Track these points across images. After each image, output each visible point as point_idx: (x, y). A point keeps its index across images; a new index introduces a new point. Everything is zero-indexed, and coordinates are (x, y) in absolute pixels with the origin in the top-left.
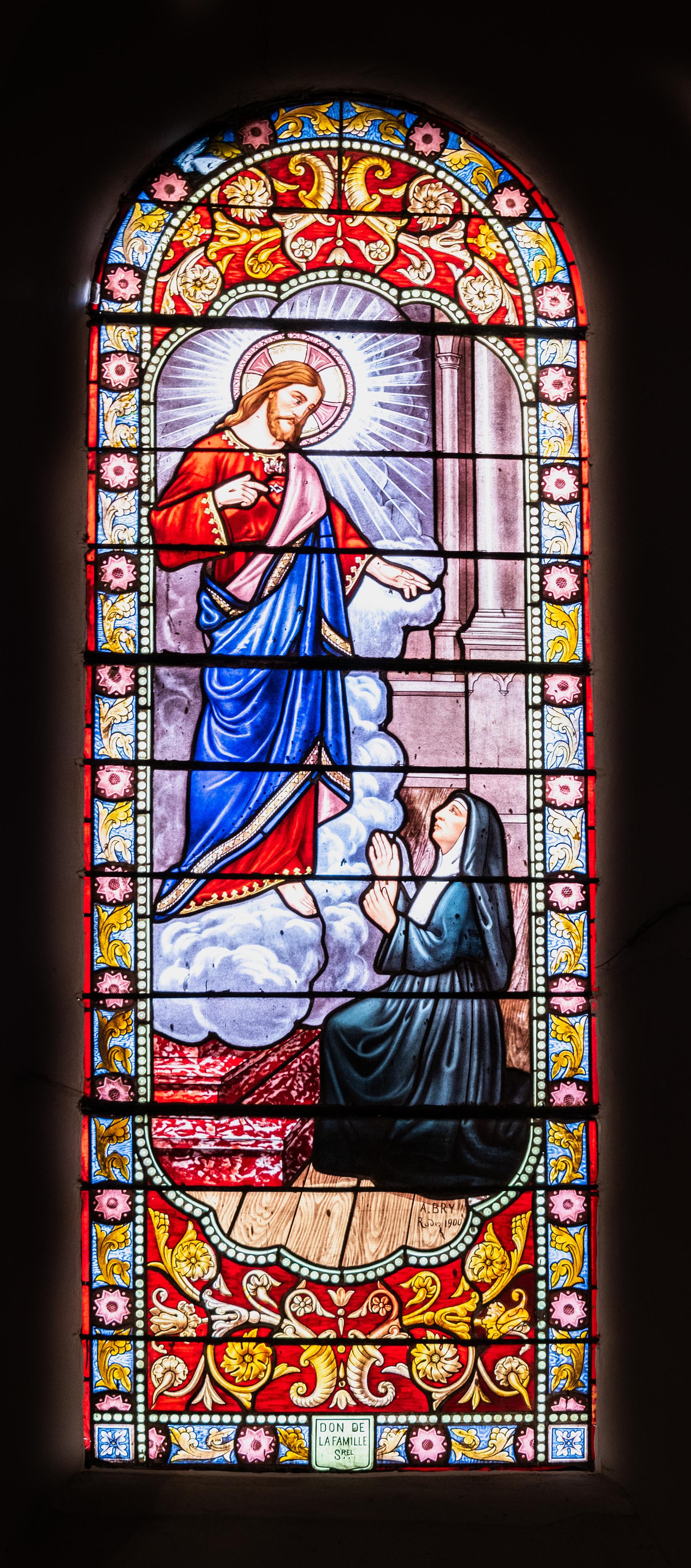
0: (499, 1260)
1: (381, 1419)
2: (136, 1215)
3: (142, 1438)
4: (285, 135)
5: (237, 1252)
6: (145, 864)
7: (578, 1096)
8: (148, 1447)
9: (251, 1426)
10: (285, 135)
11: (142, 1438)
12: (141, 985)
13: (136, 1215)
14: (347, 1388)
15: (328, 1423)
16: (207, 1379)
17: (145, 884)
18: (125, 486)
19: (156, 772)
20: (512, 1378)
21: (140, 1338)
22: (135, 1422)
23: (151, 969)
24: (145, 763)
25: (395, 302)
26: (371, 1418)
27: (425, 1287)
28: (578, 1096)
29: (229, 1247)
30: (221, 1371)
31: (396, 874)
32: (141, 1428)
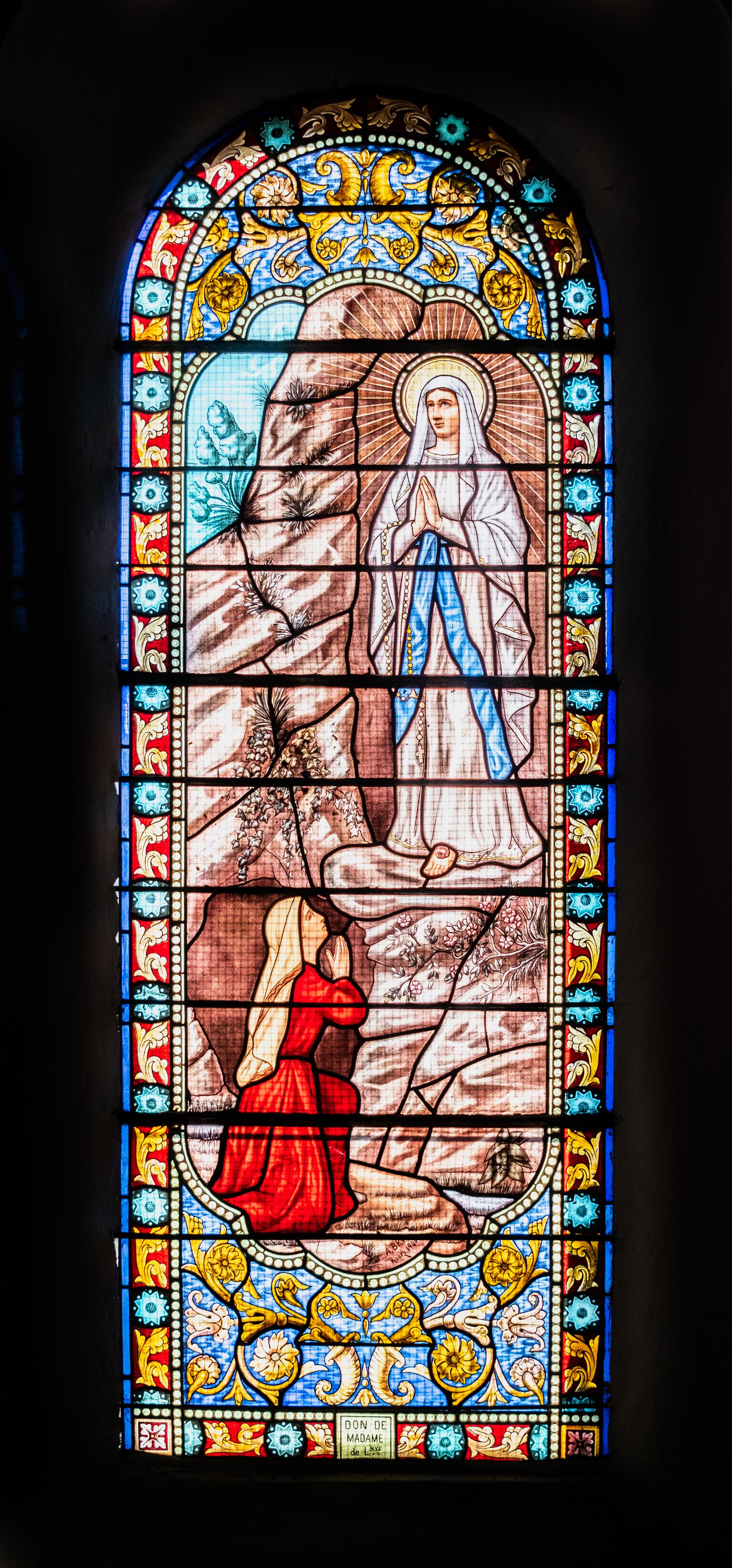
0: (516, 1264)
1: (401, 1417)
2: (173, 1320)
3: (178, 1432)
4: (308, 135)
5: (266, 1256)
6: (180, 768)
7: (591, 1102)
8: (184, 1441)
9: (280, 1422)
10: (308, 135)
11: (178, 1432)
12: (176, 459)
13: (173, 1320)
14: (370, 1388)
15: (352, 1420)
16: (238, 1376)
17: (180, 788)
18: (157, 313)
19: (190, 788)
20: (529, 1378)
21: (177, 1407)
22: (171, 1417)
23: (186, 871)
24: (180, 780)
25: (309, 1255)
26: (392, 1416)
27: (445, 1290)
28: (591, 1102)
29: (258, 1252)
30: (250, 1370)
31: (429, 790)
32: (177, 1422)
